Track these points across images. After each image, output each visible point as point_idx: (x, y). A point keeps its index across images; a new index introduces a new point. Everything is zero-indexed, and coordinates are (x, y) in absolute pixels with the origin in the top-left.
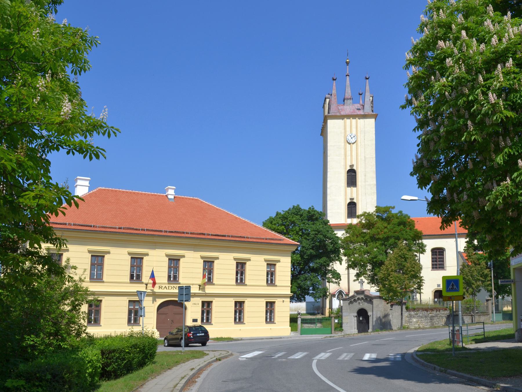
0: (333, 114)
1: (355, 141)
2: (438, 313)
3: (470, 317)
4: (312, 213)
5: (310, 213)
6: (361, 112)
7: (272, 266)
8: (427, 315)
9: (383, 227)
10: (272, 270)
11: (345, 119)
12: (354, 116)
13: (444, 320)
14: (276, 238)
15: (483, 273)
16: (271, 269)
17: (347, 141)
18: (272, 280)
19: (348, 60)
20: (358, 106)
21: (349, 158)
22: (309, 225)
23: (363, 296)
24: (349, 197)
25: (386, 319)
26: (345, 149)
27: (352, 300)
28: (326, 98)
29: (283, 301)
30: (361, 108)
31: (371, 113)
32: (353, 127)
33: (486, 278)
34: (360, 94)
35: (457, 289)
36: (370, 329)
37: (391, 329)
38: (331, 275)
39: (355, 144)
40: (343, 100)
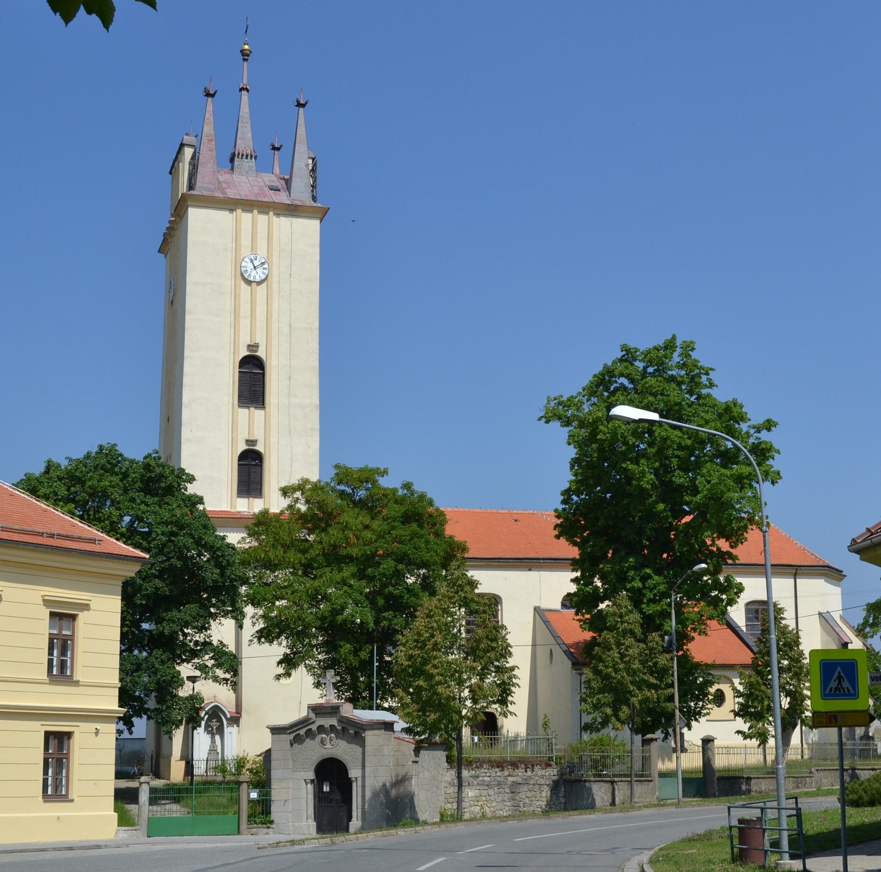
0: (204, 193)
1: (263, 277)
2: (529, 773)
3: (609, 785)
4: (158, 470)
5: (151, 471)
6: (282, 198)
7: (65, 623)
8: (502, 779)
9: (360, 527)
10: (64, 632)
11: (239, 211)
12: (264, 207)
13: (544, 794)
14: (77, 534)
15: (656, 664)
16: (60, 630)
17: (242, 275)
18: (63, 665)
19: (246, 47)
20: (271, 179)
21: (245, 323)
22: (147, 505)
23: (334, 721)
24: (243, 435)
25: (401, 790)
26: (236, 297)
27: (302, 732)
28: (182, 145)
29: (97, 732)
30: (280, 187)
31: (309, 202)
32: (259, 235)
33: (663, 677)
34: (274, 148)
35: (852, 691)
36: (354, 819)
37: (417, 821)
38: (211, 658)
39: (264, 285)
40: (228, 157)
